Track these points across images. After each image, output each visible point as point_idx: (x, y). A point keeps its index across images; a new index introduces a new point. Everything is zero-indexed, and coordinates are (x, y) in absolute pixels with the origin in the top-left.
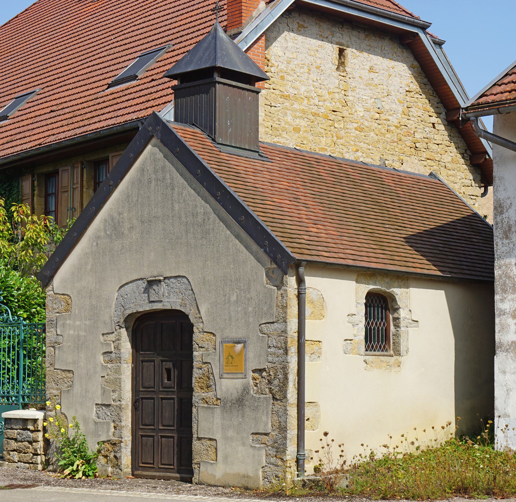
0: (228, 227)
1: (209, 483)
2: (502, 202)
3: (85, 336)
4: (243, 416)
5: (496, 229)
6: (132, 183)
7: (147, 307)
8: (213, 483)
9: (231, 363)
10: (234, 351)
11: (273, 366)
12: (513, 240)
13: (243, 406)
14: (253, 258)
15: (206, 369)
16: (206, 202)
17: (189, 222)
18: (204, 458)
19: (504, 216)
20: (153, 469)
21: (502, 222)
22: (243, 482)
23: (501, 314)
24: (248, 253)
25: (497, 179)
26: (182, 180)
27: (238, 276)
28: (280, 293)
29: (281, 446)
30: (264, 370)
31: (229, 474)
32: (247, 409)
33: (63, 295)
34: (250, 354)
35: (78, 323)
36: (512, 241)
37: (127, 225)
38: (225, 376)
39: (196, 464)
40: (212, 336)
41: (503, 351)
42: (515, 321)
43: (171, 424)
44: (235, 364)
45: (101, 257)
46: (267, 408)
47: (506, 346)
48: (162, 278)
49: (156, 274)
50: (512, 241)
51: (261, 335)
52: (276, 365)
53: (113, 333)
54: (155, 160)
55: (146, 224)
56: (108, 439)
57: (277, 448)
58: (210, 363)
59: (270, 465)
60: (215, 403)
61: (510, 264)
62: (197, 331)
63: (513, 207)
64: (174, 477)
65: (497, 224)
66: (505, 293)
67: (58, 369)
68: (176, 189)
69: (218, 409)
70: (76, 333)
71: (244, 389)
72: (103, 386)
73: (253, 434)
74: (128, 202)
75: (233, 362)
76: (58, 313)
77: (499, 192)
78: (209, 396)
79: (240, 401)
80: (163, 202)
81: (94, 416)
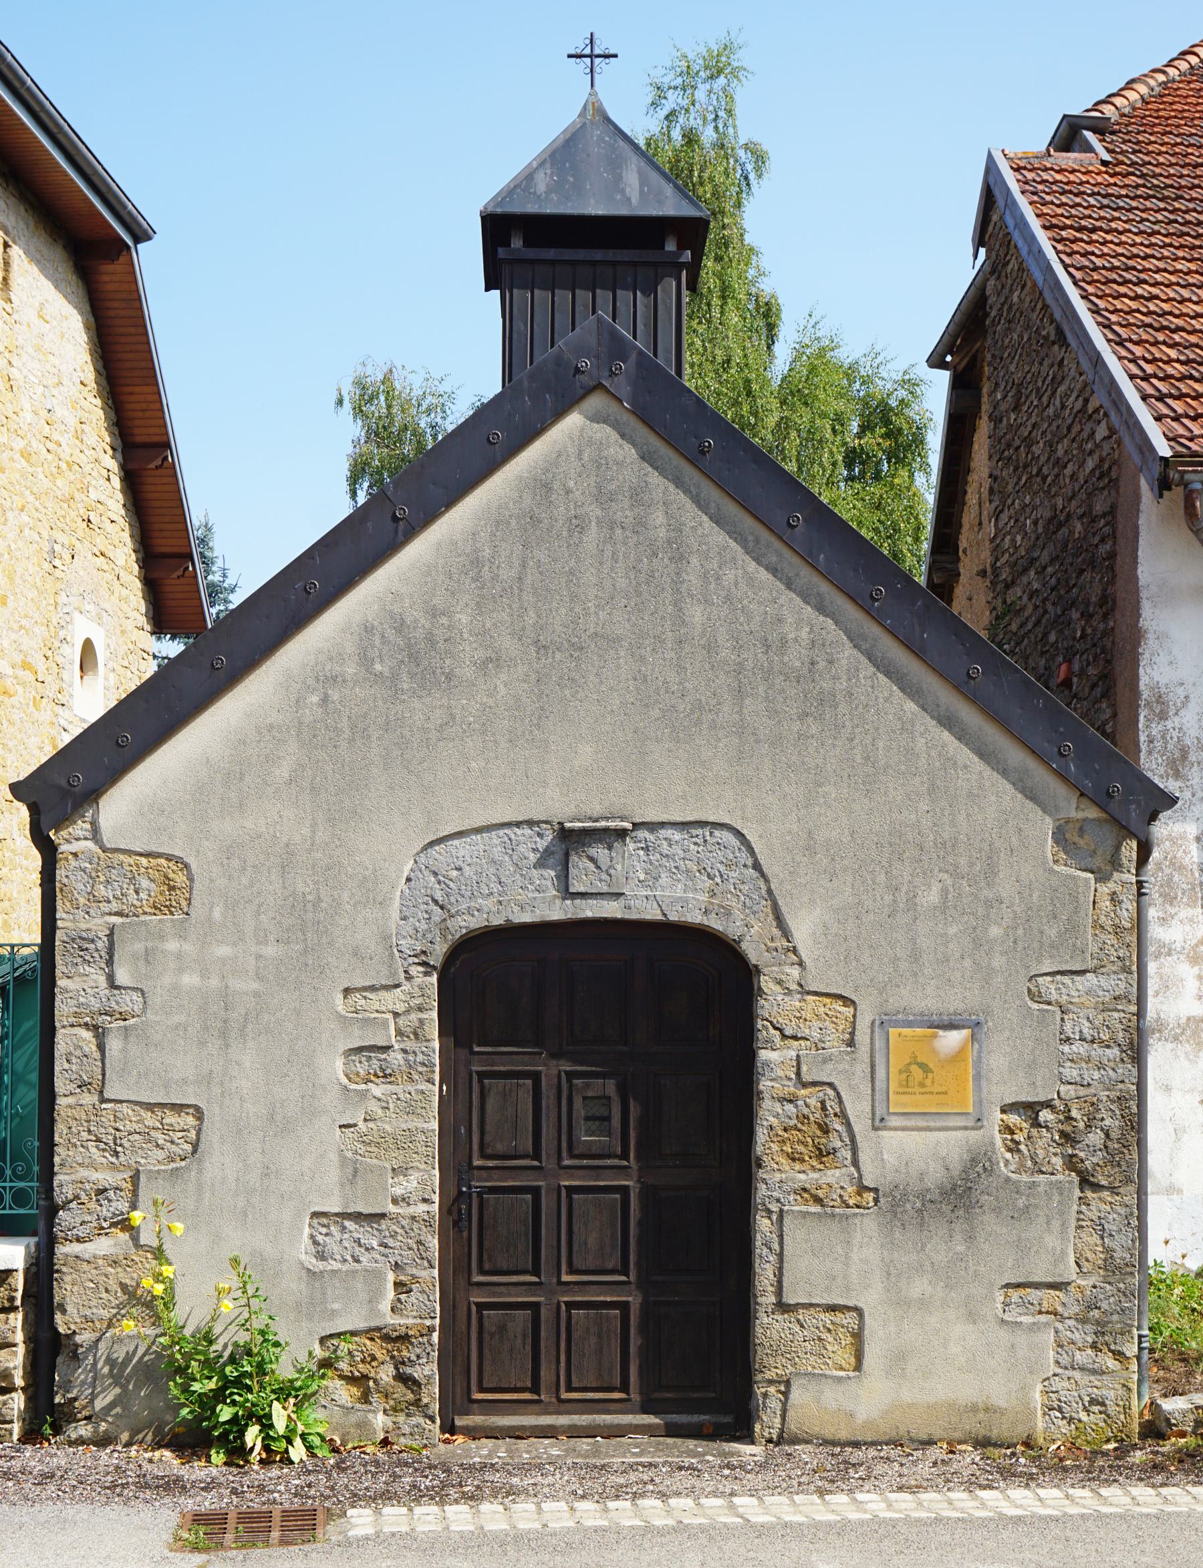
0: (910, 689)
1: (829, 1437)
2: (1163, 690)
3: (256, 994)
4: (970, 1238)
5: (1150, 753)
6: (498, 522)
7: (558, 911)
8: (843, 1435)
9: (922, 1085)
10: (934, 1052)
11: (1081, 1094)
12: (1193, 782)
13: (968, 1208)
14: (1009, 786)
15: (813, 1102)
16: (821, 609)
17: (749, 664)
18: (809, 1364)
19: (1169, 724)
20: (536, 1407)
21: (1163, 737)
22: (972, 1425)
23: (1160, 954)
24: (988, 772)
25: (1150, 636)
26: (719, 537)
27: (946, 836)
28: (1104, 889)
29: (1115, 1317)
30: (1048, 1105)
31: (910, 1406)
32: (989, 1218)
33: (147, 855)
34: (998, 1060)
35: (223, 951)
36: (1189, 783)
37: (470, 651)
38: (894, 1121)
39: (771, 1382)
40: (838, 1006)
41: (1166, 1040)
42: (1196, 970)
43: (610, 1266)
44: (936, 1089)
45: (344, 745)
46: (1061, 1213)
47: (1173, 1029)
48: (629, 826)
49: (597, 809)
50: (1189, 783)
51: (1035, 1006)
52: (1092, 1091)
53: (397, 986)
54: (600, 463)
55: (558, 656)
56: (373, 1324)
57: (1098, 1323)
58: (831, 1085)
59: (1070, 1373)
60: (851, 1202)
61: (1183, 836)
62: (777, 989)
63: (1192, 705)
64: (637, 1426)
65: (1152, 742)
66: (1171, 904)
67: (121, 1102)
68: (695, 561)
69: (866, 1220)
70: (214, 982)
71: (973, 1160)
72: (349, 1154)
73: (1007, 1286)
74: (474, 580)
75: (928, 1082)
76: (119, 914)
77: (1155, 667)
78: (830, 1180)
79: (959, 1195)
80: (639, 594)
81: (303, 1252)
